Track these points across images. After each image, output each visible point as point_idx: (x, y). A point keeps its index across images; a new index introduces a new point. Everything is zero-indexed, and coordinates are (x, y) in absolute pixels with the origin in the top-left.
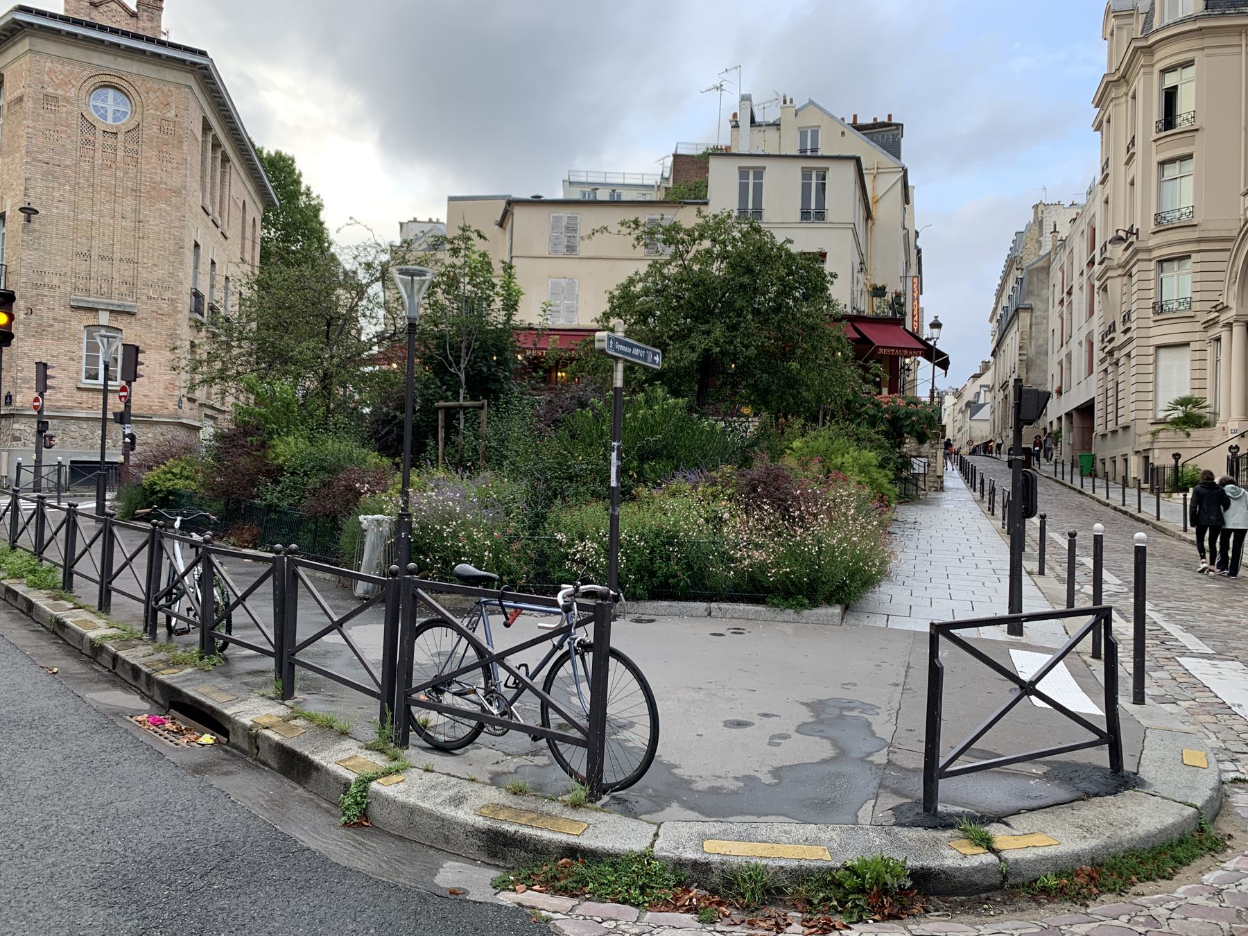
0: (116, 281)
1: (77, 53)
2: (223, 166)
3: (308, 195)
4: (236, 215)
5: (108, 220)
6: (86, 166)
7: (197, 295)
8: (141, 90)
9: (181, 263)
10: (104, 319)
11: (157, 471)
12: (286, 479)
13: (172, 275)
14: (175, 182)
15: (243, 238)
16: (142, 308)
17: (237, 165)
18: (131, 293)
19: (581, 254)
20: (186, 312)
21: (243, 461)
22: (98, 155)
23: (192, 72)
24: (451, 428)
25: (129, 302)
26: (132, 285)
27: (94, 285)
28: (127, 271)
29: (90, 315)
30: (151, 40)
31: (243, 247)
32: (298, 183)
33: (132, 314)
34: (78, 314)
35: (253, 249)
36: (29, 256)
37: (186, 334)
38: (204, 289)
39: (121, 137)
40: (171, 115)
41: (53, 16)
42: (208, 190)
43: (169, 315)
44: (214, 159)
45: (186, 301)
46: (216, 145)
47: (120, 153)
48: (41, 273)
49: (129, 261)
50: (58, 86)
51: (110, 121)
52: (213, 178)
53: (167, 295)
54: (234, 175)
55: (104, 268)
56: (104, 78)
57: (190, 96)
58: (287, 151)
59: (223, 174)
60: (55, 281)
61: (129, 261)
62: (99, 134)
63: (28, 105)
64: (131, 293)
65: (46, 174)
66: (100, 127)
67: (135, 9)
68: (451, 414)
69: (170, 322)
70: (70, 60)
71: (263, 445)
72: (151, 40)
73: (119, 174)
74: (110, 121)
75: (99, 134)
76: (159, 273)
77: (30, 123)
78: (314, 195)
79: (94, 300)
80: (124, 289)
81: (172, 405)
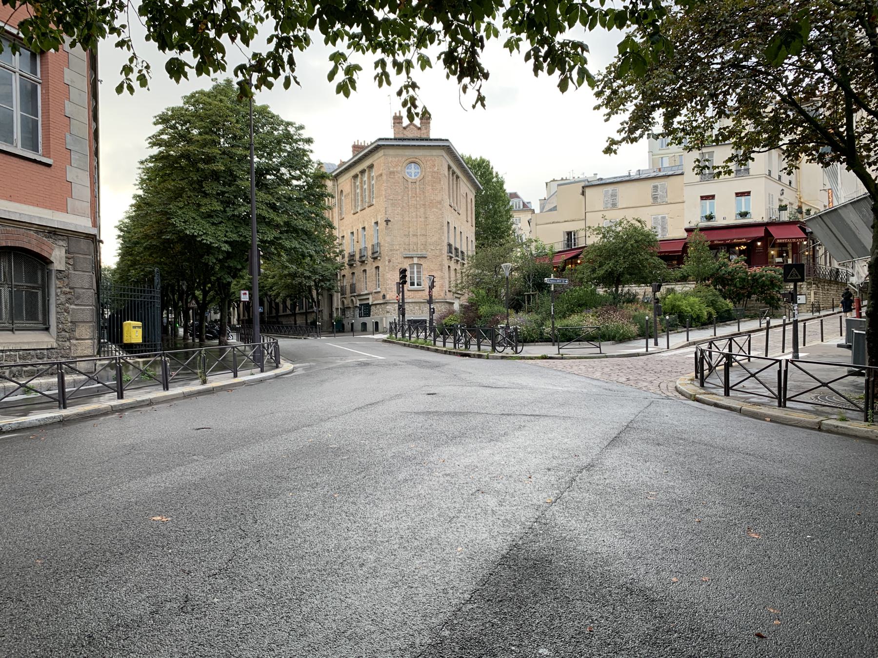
0: (419, 244)
1: (400, 152)
2: (457, 180)
3: (497, 176)
4: (463, 201)
5: (415, 219)
6: (405, 198)
7: (450, 245)
8: (424, 162)
9: (443, 233)
10: (416, 261)
11: (447, 319)
12: (483, 319)
13: (440, 239)
14: (439, 198)
15: (467, 210)
16: (429, 254)
17: (465, 181)
18: (425, 249)
19: (620, 207)
20: (446, 254)
21: (471, 314)
22: (410, 192)
23: (443, 149)
24: (529, 301)
25: (424, 252)
26: (425, 245)
27: (411, 247)
28: (422, 240)
29: (411, 260)
30: (427, 140)
31: (467, 214)
32: (491, 173)
33: (426, 257)
34: (406, 260)
35: (472, 213)
36: (388, 239)
37: (446, 263)
38: (452, 242)
39: (418, 183)
40: (436, 169)
41: (391, 139)
42: (451, 191)
43: (439, 256)
44: (453, 179)
45: (446, 248)
46: (454, 173)
47: (418, 190)
48: (392, 245)
49: (423, 235)
50: (394, 167)
51: (413, 177)
52: (453, 188)
53: (438, 247)
54: (461, 183)
55: (414, 240)
56: (410, 160)
57: (443, 159)
58: (486, 157)
59: (457, 184)
60: (398, 248)
61: (423, 235)
62: (410, 183)
63: (384, 177)
64: (425, 249)
65: (392, 204)
66: (410, 181)
67: (419, 126)
68: (529, 296)
69: (440, 259)
70: (397, 156)
71: (477, 309)
72: (427, 140)
73: (418, 199)
74: (413, 177)
75: (410, 183)
76: (435, 239)
77: (385, 185)
78: (500, 176)
79: (412, 253)
80: (422, 247)
81: (443, 294)
